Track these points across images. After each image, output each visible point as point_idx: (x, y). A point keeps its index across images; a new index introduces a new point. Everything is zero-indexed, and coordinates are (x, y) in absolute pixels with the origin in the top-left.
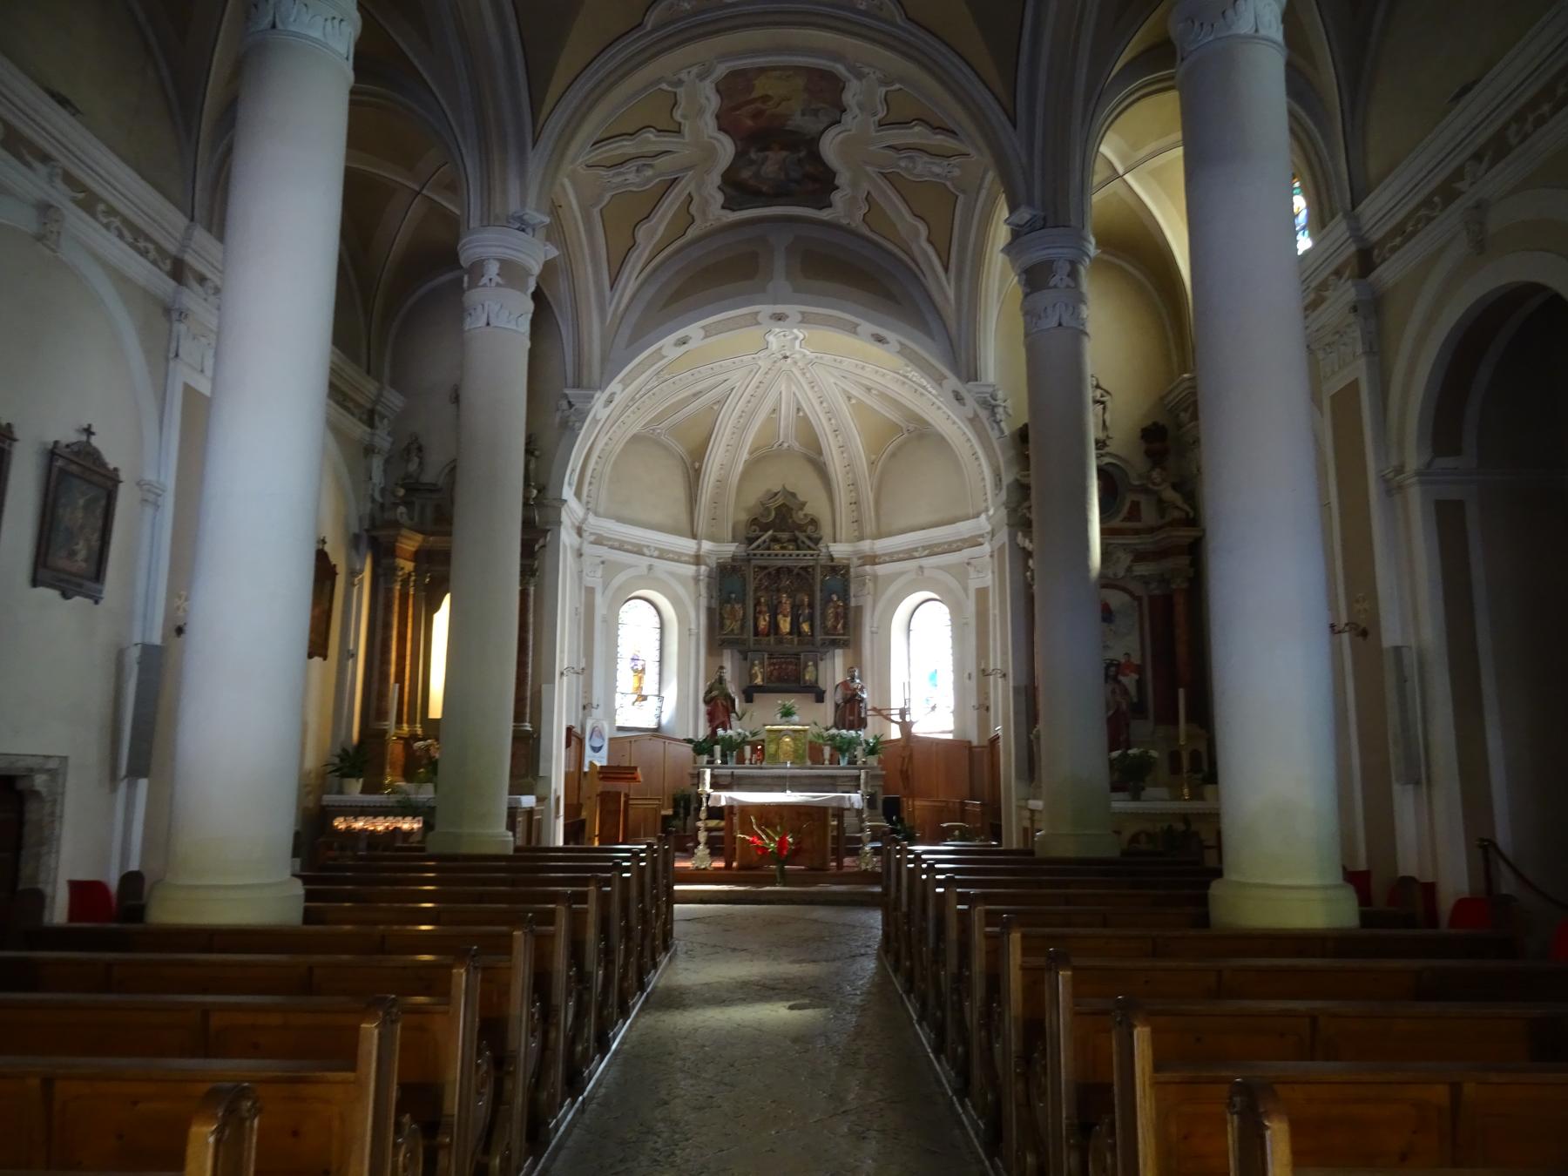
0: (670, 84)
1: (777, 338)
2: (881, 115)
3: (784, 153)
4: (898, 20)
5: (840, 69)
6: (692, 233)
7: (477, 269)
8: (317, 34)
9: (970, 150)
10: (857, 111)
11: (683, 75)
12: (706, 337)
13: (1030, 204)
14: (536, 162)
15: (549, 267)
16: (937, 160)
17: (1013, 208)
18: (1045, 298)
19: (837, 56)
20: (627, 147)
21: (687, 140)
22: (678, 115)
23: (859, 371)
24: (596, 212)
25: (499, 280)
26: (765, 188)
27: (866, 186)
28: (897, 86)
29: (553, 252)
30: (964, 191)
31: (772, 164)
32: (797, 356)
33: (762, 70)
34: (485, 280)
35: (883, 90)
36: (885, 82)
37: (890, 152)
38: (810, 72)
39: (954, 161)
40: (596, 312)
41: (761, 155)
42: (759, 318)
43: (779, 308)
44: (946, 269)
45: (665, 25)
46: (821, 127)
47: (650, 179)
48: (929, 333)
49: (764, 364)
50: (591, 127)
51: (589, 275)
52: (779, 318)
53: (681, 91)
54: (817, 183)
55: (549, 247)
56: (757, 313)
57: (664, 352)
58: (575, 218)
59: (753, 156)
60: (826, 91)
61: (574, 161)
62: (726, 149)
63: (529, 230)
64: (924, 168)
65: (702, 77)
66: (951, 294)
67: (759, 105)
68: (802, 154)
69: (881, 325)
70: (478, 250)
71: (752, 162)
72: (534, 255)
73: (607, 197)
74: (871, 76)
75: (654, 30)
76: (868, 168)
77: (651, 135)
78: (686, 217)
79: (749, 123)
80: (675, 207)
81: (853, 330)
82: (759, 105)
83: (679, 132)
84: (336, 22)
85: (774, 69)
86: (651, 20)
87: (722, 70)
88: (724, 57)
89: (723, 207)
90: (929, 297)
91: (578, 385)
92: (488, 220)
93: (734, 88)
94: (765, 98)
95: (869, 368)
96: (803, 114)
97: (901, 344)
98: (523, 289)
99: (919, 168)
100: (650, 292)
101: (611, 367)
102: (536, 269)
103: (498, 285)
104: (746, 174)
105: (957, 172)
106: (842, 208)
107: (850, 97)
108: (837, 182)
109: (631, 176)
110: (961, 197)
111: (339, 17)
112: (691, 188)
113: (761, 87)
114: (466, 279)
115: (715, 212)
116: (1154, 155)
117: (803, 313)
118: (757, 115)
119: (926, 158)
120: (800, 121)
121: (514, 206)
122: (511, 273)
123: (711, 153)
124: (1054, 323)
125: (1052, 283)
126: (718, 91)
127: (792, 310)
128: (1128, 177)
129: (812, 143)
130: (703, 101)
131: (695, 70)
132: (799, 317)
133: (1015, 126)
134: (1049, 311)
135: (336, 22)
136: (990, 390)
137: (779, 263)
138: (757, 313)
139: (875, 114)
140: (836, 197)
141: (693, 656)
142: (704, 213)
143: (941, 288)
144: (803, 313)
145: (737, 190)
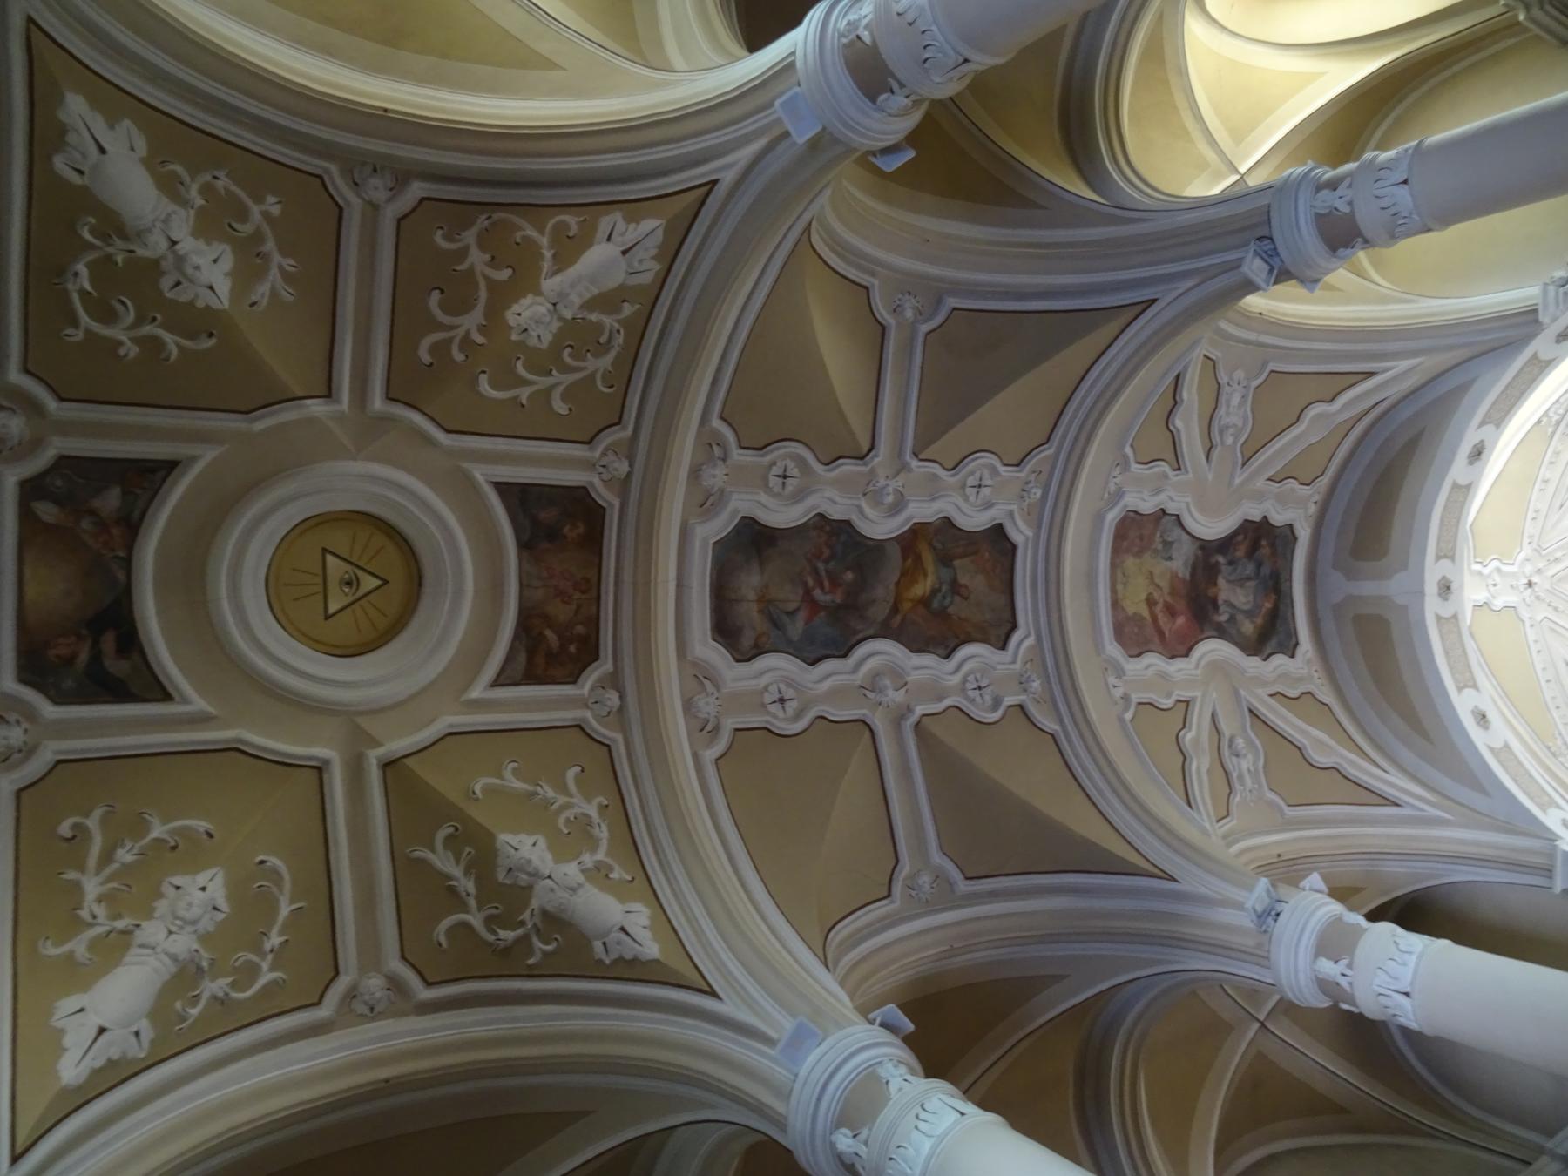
0: (1126, 709)
1: (1472, 593)
2: (1164, 467)
3: (1221, 581)
4: (1052, 451)
5: (1113, 516)
6: (1327, 696)
7: (1325, 985)
8: (927, 1145)
9: (1197, 355)
10: (1162, 497)
11: (1118, 693)
12: (1475, 687)
13: (1236, 265)
14: (1193, 881)
15: (1340, 893)
16: (1223, 399)
17: (1250, 287)
18: (1367, 218)
19: (1099, 518)
20: (1200, 765)
21: (1198, 694)
22: (1167, 703)
23: (1551, 488)
24: (1290, 812)
25: (1344, 962)
26: (1268, 605)
27: (1260, 483)
28: (1128, 450)
29: (1315, 880)
30: (1265, 364)
31: (1235, 595)
32: (1528, 569)
33: (1115, 604)
34: (1343, 982)
35: (1135, 467)
36: (1124, 464)
37: (1216, 454)
38: (1117, 550)
39: (1223, 379)
40: (1423, 833)
41: (1222, 609)
42: (1446, 613)
43: (1431, 588)
44: (1371, 374)
45: (1057, 710)
46: (1185, 537)
47: (1250, 743)
48: (1464, 388)
49: (1542, 612)
50: (1166, 807)
51: (1372, 832)
52: (1445, 588)
53: (1135, 697)
54: (1261, 542)
55: (1305, 883)
56: (1439, 618)
57: (1498, 745)
58: (1295, 840)
59: (1223, 618)
60: (1138, 533)
61: (1204, 832)
62: (1213, 649)
63: (1279, 907)
64: (1235, 413)
65: (1120, 673)
66: (1404, 364)
67: (1159, 608)
68: (1221, 559)
69: (1453, 452)
70: (1302, 976)
71: (1232, 619)
72: (1312, 906)
73: (1271, 796)
74: (1113, 480)
75: (1061, 722)
76: (1237, 481)
77: (1188, 737)
78: (1302, 702)
79: (1181, 621)
80: (1289, 715)
81: (1464, 491)
82: (1159, 608)
83: (1188, 702)
84: (923, 1115)
85: (1114, 591)
86: (1051, 725)
87: (1113, 650)
88: (1098, 646)
89: (1292, 656)
90: (1415, 391)
91: (1549, 872)
92: (1262, 958)
93: (1135, 635)
94: (1151, 602)
95: (1545, 472)
96: (1170, 558)
97: (1483, 423)
98: (1358, 932)
99: (1235, 420)
100: (1406, 755)
101: (1521, 822)
102: (1336, 908)
103: (1350, 966)
104: (1248, 628)
105: (1240, 374)
106: (1294, 511)
107: (1147, 506)
108: (1257, 519)
109: (1245, 766)
110: (1271, 366)
111: (918, 1109)
112: (1263, 692)
113: (1135, 605)
114: (1345, 1006)
115: (1299, 667)
116: (1213, 142)
117: (1438, 558)
118: (1171, 612)
119: (1222, 411)
120: (1180, 562)
121: (1246, 921)
122: (1333, 943)
123: (1218, 668)
124: (1404, 189)
125: (1347, 209)
126: (1139, 655)
127: (1433, 572)
128: (1243, 170)
129: (1207, 549)
130: (1151, 672)
131: (1112, 680)
132: (1445, 562)
133: (1154, 301)
134: (1384, 203)
135: (923, 1115)
136: (1552, 289)
137: (1367, 588)
138: (1439, 618)
139: (1166, 476)
140: (1278, 519)
141: (679, 326)
142: (1300, 680)
143: (1394, 379)
144: (1438, 558)
145: (1270, 635)
